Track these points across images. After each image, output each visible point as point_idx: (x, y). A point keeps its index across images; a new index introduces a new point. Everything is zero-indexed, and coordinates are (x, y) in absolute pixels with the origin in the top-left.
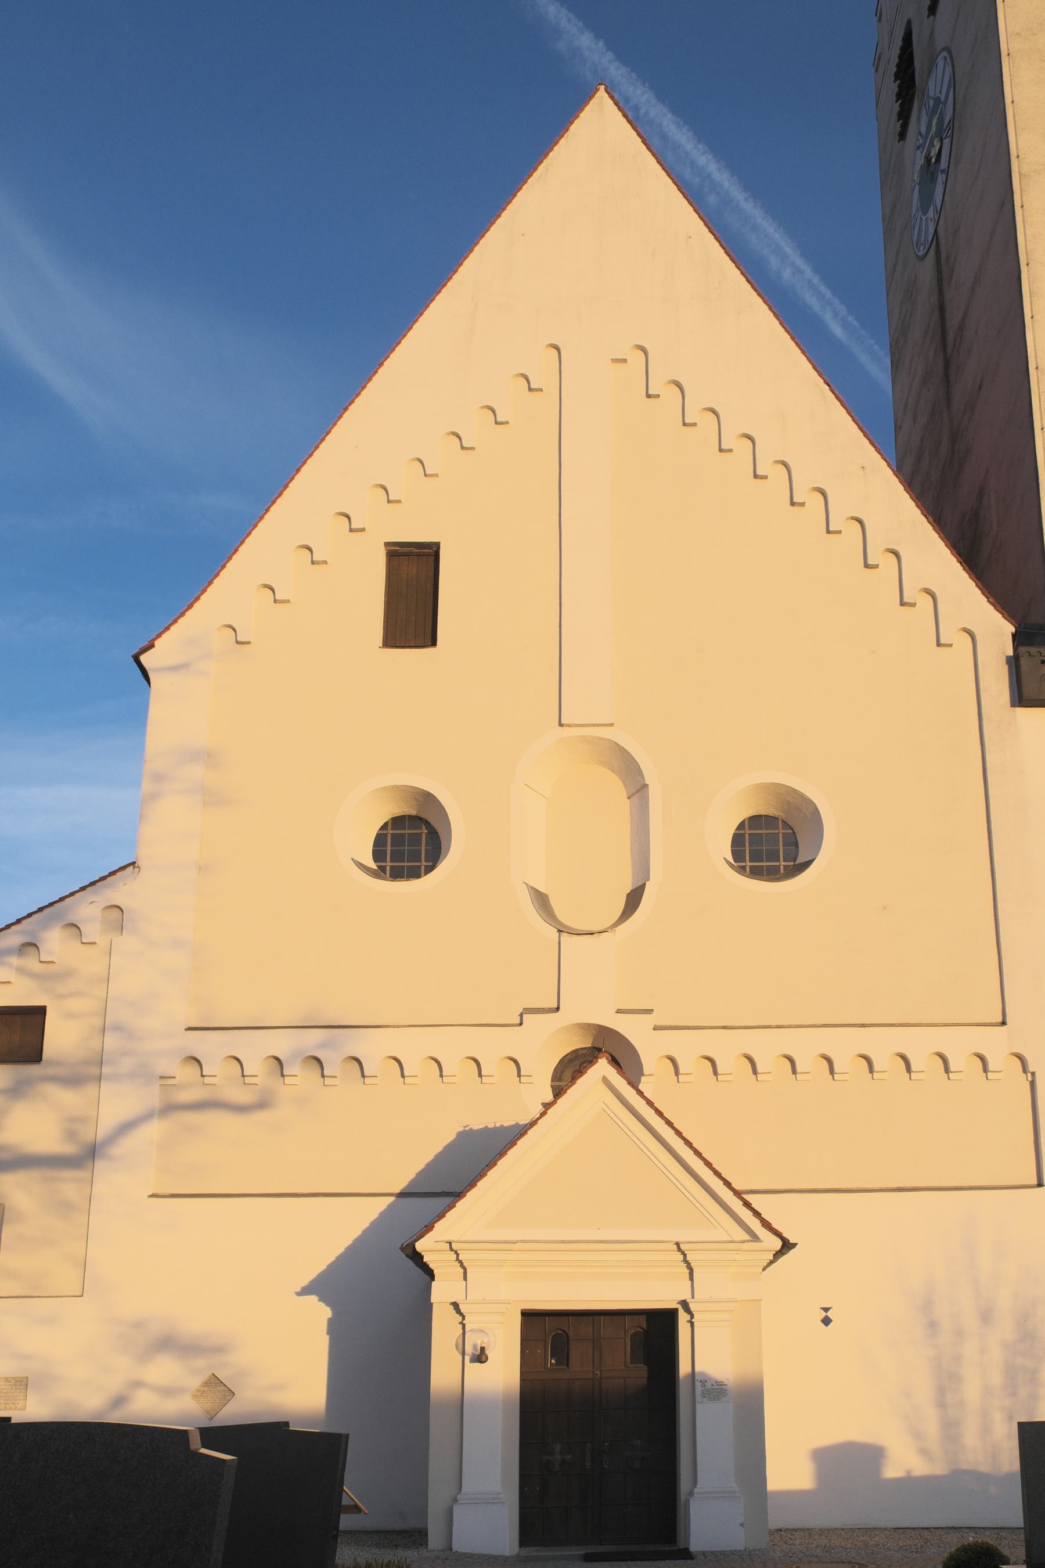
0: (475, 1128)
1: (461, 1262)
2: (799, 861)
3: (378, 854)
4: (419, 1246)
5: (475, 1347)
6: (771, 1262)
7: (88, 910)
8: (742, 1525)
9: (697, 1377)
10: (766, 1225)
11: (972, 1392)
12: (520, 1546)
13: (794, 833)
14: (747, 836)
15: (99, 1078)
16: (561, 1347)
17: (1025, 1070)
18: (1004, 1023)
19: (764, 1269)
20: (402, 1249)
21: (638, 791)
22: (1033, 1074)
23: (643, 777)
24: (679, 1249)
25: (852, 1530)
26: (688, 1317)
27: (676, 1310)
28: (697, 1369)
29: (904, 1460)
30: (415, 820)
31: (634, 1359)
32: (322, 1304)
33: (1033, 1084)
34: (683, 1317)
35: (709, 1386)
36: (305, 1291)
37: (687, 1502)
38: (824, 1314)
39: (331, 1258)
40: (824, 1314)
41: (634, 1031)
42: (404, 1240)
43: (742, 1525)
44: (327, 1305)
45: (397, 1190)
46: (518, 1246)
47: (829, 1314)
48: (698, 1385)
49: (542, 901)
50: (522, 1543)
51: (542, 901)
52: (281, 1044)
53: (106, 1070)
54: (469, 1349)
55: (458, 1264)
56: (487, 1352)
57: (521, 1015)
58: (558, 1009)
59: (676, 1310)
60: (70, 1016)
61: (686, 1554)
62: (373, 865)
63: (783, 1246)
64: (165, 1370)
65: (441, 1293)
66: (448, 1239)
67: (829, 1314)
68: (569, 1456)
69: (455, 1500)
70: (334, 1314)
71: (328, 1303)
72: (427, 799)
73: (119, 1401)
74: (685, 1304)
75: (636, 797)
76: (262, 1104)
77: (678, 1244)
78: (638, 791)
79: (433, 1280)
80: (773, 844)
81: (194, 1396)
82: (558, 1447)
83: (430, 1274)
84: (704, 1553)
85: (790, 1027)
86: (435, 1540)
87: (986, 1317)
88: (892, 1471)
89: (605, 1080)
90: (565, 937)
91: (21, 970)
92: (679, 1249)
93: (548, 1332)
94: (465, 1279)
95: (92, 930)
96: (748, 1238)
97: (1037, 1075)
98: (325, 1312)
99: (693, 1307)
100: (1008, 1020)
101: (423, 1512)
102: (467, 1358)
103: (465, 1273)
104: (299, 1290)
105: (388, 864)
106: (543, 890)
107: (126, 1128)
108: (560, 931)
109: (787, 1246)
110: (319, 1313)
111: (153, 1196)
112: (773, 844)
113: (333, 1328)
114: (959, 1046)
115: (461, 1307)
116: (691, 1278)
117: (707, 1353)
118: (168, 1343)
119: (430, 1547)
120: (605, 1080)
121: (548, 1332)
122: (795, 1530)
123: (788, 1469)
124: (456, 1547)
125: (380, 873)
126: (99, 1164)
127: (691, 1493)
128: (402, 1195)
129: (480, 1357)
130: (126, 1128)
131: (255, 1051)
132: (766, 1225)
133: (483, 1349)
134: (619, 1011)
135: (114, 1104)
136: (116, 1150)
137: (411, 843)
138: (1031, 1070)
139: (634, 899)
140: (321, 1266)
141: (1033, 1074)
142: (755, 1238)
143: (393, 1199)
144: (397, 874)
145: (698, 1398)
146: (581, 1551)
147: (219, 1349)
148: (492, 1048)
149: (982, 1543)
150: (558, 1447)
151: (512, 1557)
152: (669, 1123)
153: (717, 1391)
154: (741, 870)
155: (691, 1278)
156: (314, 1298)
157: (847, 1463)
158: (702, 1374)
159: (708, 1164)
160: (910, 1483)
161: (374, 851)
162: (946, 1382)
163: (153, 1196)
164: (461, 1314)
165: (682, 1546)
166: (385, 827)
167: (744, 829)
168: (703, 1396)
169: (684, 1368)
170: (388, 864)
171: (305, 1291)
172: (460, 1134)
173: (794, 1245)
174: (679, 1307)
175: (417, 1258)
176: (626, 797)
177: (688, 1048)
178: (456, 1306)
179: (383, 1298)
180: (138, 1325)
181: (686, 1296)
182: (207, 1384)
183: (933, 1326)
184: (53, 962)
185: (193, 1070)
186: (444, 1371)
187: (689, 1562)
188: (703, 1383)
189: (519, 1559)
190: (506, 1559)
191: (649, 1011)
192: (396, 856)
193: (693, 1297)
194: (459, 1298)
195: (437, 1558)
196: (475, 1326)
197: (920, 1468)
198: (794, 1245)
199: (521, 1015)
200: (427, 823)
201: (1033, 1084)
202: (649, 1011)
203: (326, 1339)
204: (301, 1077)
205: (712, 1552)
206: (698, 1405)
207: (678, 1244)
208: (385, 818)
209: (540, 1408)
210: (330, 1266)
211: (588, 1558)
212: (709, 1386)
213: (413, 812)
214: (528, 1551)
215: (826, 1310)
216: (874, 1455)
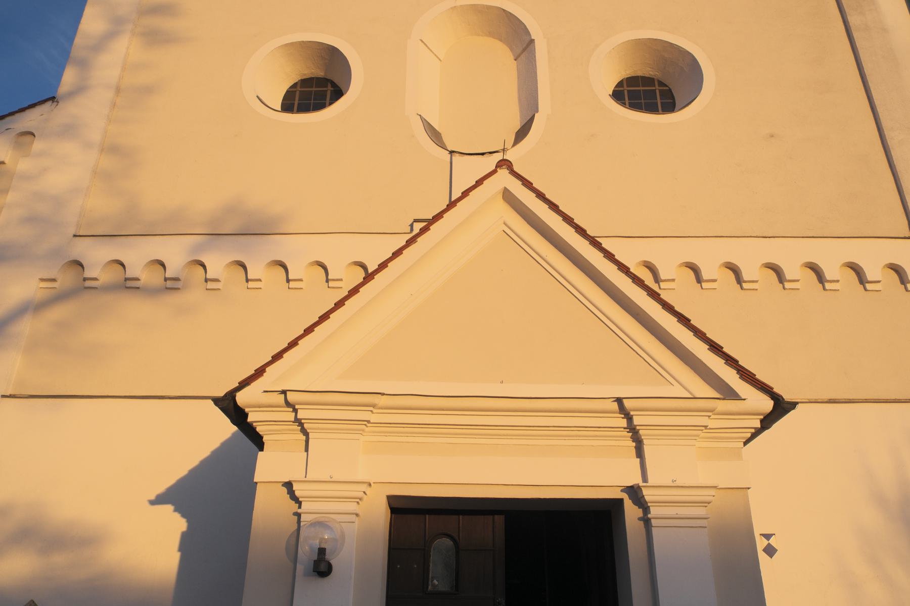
1: (298, 422)
4: (242, 398)
6: (757, 433)
10: (747, 376)
13: (670, 90)
14: (626, 93)
19: (745, 443)
21: (524, 50)
23: (530, 34)
24: (622, 409)
26: (639, 512)
27: (620, 502)
32: (177, 516)
34: (631, 512)
36: (159, 500)
38: (765, 542)
40: (765, 542)
44: (183, 516)
51: (435, 136)
56: (328, 557)
57: (412, 226)
59: (620, 502)
67: (772, 542)
70: (189, 527)
75: (522, 56)
77: (619, 401)
78: (524, 50)
79: (261, 449)
80: (655, 88)
83: (258, 442)
90: (456, 158)
92: (622, 409)
94: (307, 450)
98: (180, 524)
102: (300, 568)
104: (153, 497)
109: (782, 407)
110: (172, 524)
112: (655, 88)
113: (187, 544)
115: (295, 487)
116: (640, 452)
120: (508, 196)
132: (747, 376)
133: (322, 551)
137: (318, 88)
140: (182, 471)
142: (729, 394)
155: (640, 452)
156: (169, 508)
166: (295, 85)
167: (622, 86)
171: (159, 500)
174: (625, 496)
176: (512, 57)
178: (289, 485)
181: (635, 479)
193: (645, 479)
198: (793, 405)
207: (619, 401)
208: (295, 79)
213: (321, 74)
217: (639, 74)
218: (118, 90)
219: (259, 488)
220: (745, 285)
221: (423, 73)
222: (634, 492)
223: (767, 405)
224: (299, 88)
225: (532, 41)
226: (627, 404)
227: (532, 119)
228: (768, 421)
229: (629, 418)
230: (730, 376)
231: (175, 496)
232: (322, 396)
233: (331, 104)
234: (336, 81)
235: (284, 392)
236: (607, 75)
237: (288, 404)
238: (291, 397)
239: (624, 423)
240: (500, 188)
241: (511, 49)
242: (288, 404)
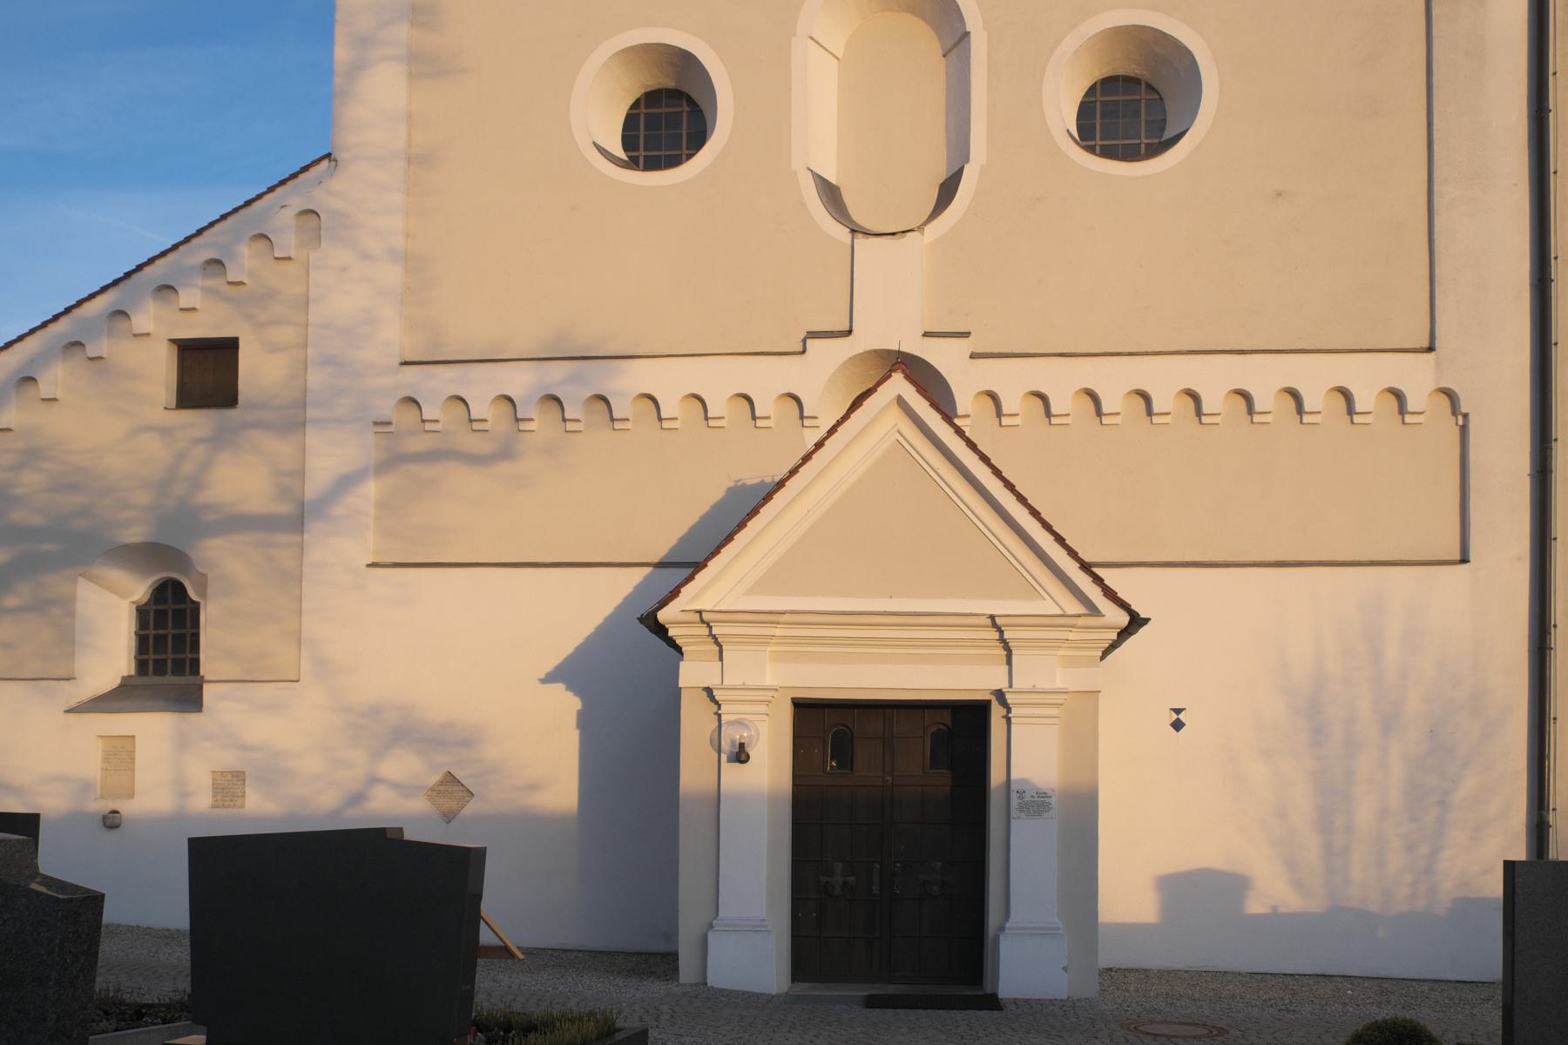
0: (749, 482)
1: (714, 637)
2: (1167, 135)
3: (628, 142)
4: (663, 616)
5: (733, 742)
6: (1114, 646)
7: (282, 214)
8: (1065, 969)
9: (1013, 787)
10: (1110, 594)
11: (1364, 814)
12: (793, 981)
15: (304, 424)
16: (843, 749)
17: (1455, 411)
18: (1431, 349)
19: (1106, 653)
20: (642, 620)
21: (956, 45)
22: (1465, 416)
24: (994, 625)
25: (1199, 973)
26: (1004, 712)
27: (989, 702)
28: (1014, 776)
29: (1273, 890)
30: (675, 95)
31: (934, 763)
32: (570, 694)
33: (1464, 430)
34: (997, 712)
35: (1027, 798)
36: (550, 678)
37: (997, 939)
38: (1175, 716)
39: (579, 639)
40: (1175, 716)
41: (945, 358)
42: (644, 609)
43: (1065, 969)
45: (656, 558)
46: (786, 618)
47: (1182, 716)
48: (1014, 796)
49: (831, 194)
50: (795, 977)
51: (831, 194)
52: (520, 381)
53: (311, 413)
54: (725, 745)
55: (710, 640)
56: (748, 749)
57: (804, 341)
58: (850, 332)
59: (989, 702)
60: (273, 348)
61: (992, 1002)
62: (622, 155)
63: (1130, 623)
64: (402, 766)
65: (693, 673)
66: (698, 608)
67: (1182, 716)
68: (852, 879)
69: (711, 926)
70: (584, 705)
71: (577, 692)
72: (685, 62)
73: (357, 798)
74: (1000, 694)
75: (953, 54)
76: (505, 453)
78: (956, 45)
81: (430, 798)
82: (839, 867)
83: (679, 649)
84: (1015, 1001)
85: (1147, 354)
86: (687, 973)
87: (1389, 723)
88: (1255, 906)
89: (901, 402)
90: (860, 241)
91: (209, 292)
92: (994, 625)
93: (823, 725)
94: (721, 659)
95: (287, 242)
96: (1084, 611)
97: (1471, 417)
99: (1010, 698)
100: (1437, 344)
101: (671, 935)
102: (724, 757)
103: (721, 652)
105: (642, 153)
106: (833, 181)
107: (346, 483)
108: (853, 231)
109: (1136, 622)
110: (565, 704)
111: (373, 565)
112: (1133, 108)
113: (586, 722)
114: (1368, 378)
117: (1026, 756)
118: (405, 731)
119: (682, 980)
121: (823, 725)
122: (1129, 970)
123: (1127, 895)
124: (712, 981)
125: (633, 163)
126: (314, 529)
127: (1002, 928)
128: (661, 565)
129: (741, 756)
130: (346, 483)
131: (481, 388)
133: (742, 745)
134: (926, 334)
135: (328, 455)
136: (338, 510)
137: (668, 120)
138: (1464, 410)
139: (948, 191)
141: (1465, 416)
142: (1094, 610)
143: (648, 570)
144: (653, 164)
145: (1014, 812)
146: (862, 991)
147: (467, 742)
148: (767, 380)
149: (1405, 1020)
150: (839, 867)
151: (778, 996)
152: (985, 459)
153: (1038, 803)
154: (1091, 149)
156: (560, 687)
157: (1197, 893)
158: (1024, 781)
159: (1035, 513)
160: (1276, 920)
161: (624, 137)
162: (1332, 802)
163: (373, 565)
164: (716, 702)
165: (988, 990)
166: (636, 105)
168: (1021, 809)
169: (996, 776)
170: (642, 153)
171: (550, 678)
172: (730, 490)
173: (1146, 621)
174: (993, 698)
175: (660, 630)
176: (940, 53)
177: (1012, 381)
178: (709, 691)
179: (632, 684)
180: (375, 711)
181: (1002, 684)
182: (442, 783)
183: (1318, 733)
184: (241, 283)
185: (411, 414)
186: (695, 768)
187: (996, 1014)
188: (1021, 793)
189: (789, 1000)
190: (771, 998)
191: (966, 335)
192: (652, 143)
194: (712, 681)
195: (685, 994)
196: (733, 718)
197: (1292, 902)
198: (1146, 621)
199: (804, 341)
200: (691, 101)
201: (1464, 430)
202: (966, 335)
203: (576, 734)
204: (540, 424)
205: (1026, 1001)
206: (1014, 823)
207: (992, 617)
209: (817, 815)
210: (577, 649)
211: (872, 1002)
212: (1027, 798)
213: (671, 84)
214: (804, 988)
215: (1178, 711)
216: (1231, 886)
217: (1121, 72)
218: (409, 161)
219: (683, 692)
220: (1204, 420)
221: (813, 98)
222: (1000, 694)
223: (1123, 619)
224: (643, 110)
225: (967, 34)
226: (998, 621)
227: (961, 170)
228: (1125, 633)
229: (1001, 632)
230: (1094, 593)
231: (567, 673)
232: (732, 616)
233: (690, 157)
234: (694, 96)
235: (700, 612)
236: (1061, 107)
237: (703, 621)
238: (706, 616)
239: (996, 635)
240: (894, 395)
241: (940, 37)
242: (703, 621)
